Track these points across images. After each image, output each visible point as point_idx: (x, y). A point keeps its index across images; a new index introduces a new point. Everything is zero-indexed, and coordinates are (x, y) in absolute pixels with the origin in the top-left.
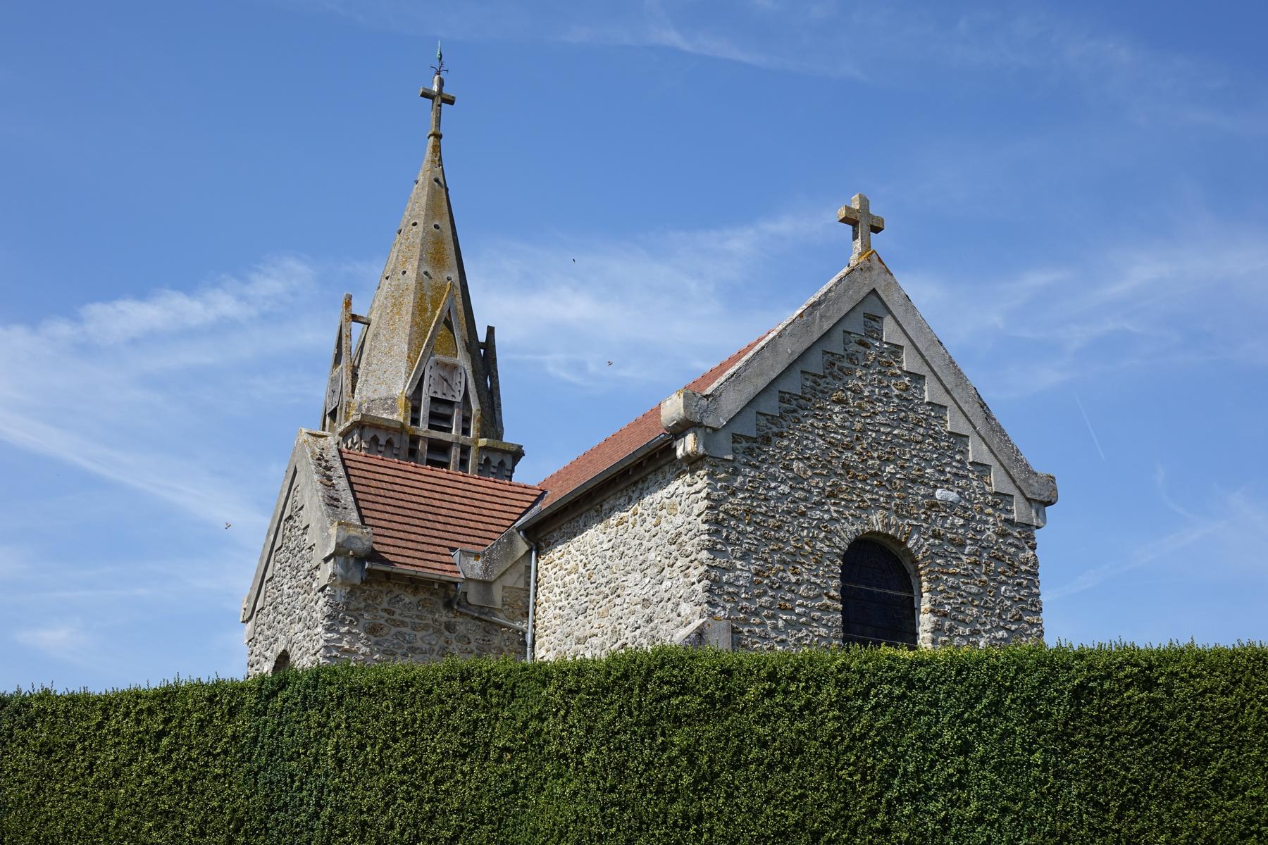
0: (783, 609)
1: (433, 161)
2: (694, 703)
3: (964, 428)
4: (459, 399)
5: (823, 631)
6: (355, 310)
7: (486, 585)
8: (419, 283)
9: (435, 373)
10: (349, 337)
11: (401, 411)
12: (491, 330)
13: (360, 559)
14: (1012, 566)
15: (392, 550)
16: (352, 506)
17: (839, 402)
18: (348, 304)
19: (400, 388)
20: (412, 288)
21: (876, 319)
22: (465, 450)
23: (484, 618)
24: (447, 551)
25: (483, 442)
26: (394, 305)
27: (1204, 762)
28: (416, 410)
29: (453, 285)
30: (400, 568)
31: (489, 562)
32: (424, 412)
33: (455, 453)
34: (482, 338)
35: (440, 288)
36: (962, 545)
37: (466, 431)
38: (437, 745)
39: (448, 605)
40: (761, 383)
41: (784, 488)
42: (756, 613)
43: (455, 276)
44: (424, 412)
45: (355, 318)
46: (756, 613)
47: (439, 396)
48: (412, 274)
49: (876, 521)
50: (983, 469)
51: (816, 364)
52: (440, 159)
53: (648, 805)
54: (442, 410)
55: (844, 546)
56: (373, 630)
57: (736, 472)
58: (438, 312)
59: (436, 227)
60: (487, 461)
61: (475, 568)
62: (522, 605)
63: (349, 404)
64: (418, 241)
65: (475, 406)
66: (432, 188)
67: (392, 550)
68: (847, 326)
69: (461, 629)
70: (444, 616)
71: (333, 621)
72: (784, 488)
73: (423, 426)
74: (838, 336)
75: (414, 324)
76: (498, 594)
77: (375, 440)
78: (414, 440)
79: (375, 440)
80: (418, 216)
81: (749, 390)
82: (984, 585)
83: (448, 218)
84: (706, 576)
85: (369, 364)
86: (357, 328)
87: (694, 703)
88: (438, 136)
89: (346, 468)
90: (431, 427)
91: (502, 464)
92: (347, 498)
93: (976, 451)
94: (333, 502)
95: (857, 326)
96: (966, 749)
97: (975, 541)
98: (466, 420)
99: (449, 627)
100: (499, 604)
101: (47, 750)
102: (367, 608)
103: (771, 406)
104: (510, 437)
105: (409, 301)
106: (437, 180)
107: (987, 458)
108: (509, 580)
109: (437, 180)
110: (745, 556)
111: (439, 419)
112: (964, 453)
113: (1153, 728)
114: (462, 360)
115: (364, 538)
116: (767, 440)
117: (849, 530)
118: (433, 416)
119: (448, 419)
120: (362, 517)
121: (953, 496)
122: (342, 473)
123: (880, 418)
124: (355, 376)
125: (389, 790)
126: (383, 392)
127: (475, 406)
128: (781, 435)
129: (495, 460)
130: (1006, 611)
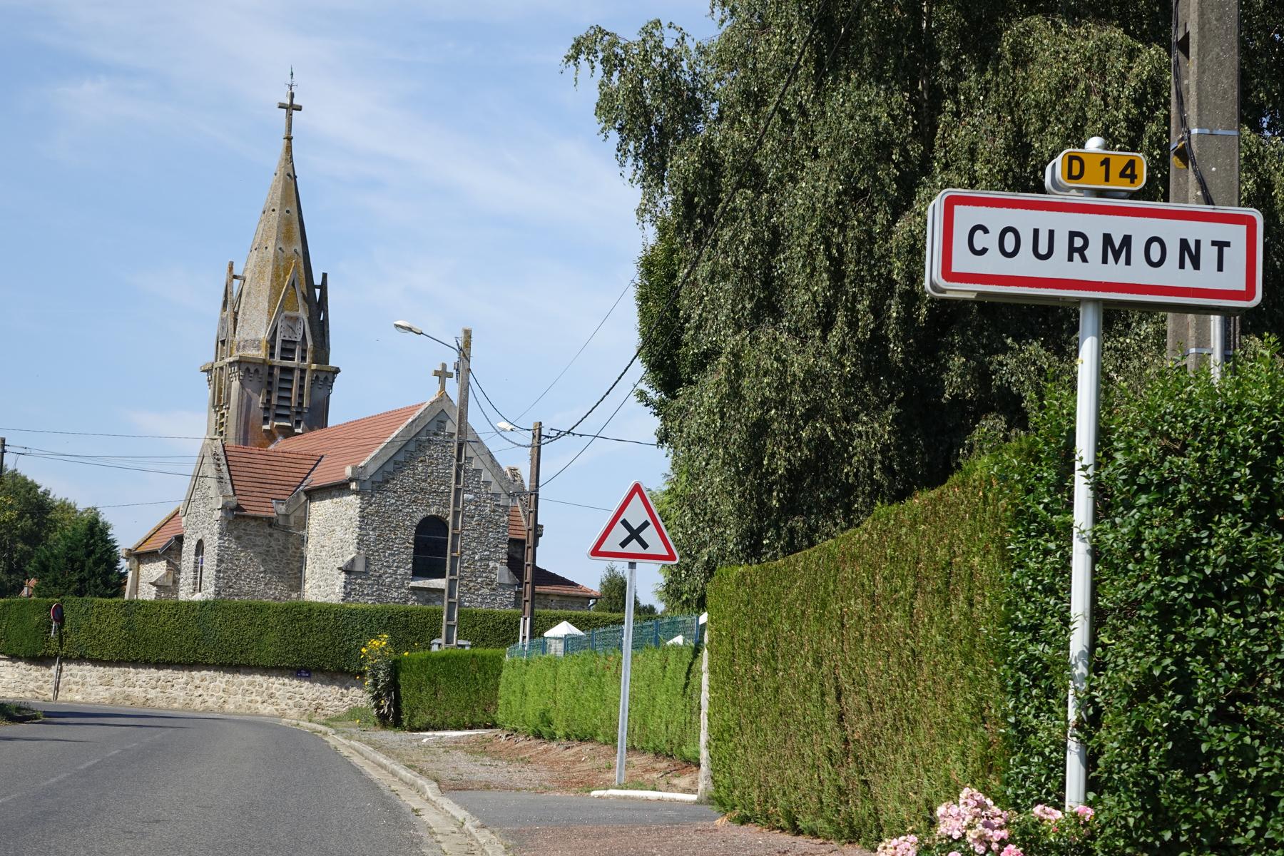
0: (389, 549)
1: (286, 159)
2: (302, 617)
3: (480, 466)
4: (299, 339)
5: (405, 556)
6: (235, 273)
7: (287, 516)
8: (276, 257)
9: (284, 324)
10: (232, 293)
11: (263, 349)
12: (325, 276)
13: (232, 510)
14: (496, 524)
15: (246, 503)
16: (229, 482)
17: (422, 461)
18: (231, 269)
19: (263, 335)
20: (271, 260)
21: (444, 422)
22: (303, 371)
23: (286, 530)
24: (270, 500)
25: (314, 366)
26: (260, 272)
27: (416, 635)
28: (273, 347)
29: (297, 265)
30: (249, 513)
31: (288, 506)
32: (277, 350)
33: (297, 374)
34: (317, 281)
35: (289, 258)
36: (473, 517)
37: (304, 359)
38: (243, 623)
39: (270, 526)
40: (386, 459)
41: (393, 501)
42: (377, 551)
43: (299, 248)
44: (277, 350)
45: (235, 277)
46: (377, 551)
47: (287, 338)
48: (271, 250)
49: (434, 511)
50: (488, 483)
51: (412, 447)
52: (291, 157)
53: (291, 640)
54: (289, 346)
55: (417, 522)
56: (238, 538)
57: (373, 496)
58: (288, 277)
59: (288, 212)
60: (317, 377)
61: (282, 509)
62: (303, 524)
63: (232, 341)
64: (276, 225)
65: (310, 343)
66: (285, 181)
67: (246, 503)
68: (428, 428)
69: (276, 536)
70: (268, 530)
71: (222, 536)
72: (393, 501)
73: (277, 360)
74: (424, 433)
75: (272, 287)
76: (292, 519)
77: (248, 369)
78: (272, 367)
79: (248, 369)
80: (275, 204)
81: (380, 463)
82: (481, 533)
83: (295, 204)
84: (357, 537)
85: (244, 314)
86: (236, 282)
87: (302, 617)
88: (289, 139)
89: (227, 461)
90: (282, 358)
91: (326, 378)
92: (227, 476)
93: (486, 476)
94: (220, 480)
95: (433, 428)
96: (362, 630)
97: (479, 515)
98: (304, 351)
99: (271, 535)
100: (292, 524)
101: (145, 616)
102: (235, 529)
103: (390, 468)
104: (333, 362)
105: (269, 270)
106: (289, 175)
107: (490, 478)
108: (297, 513)
109: (289, 175)
110: (374, 530)
111: (287, 352)
112: (480, 477)
113: (406, 626)
114: (302, 313)
115: (233, 501)
116: (387, 482)
117: (420, 516)
118: (283, 350)
119: (293, 351)
120: (234, 490)
121: (471, 497)
122: (224, 462)
123: (440, 466)
124: (236, 320)
125: (232, 632)
126: (252, 336)
127: (310, 343)
128: (393, 479)
129: (322, 377)
130: (490, 543)
